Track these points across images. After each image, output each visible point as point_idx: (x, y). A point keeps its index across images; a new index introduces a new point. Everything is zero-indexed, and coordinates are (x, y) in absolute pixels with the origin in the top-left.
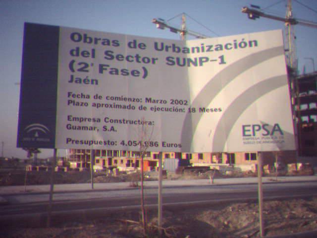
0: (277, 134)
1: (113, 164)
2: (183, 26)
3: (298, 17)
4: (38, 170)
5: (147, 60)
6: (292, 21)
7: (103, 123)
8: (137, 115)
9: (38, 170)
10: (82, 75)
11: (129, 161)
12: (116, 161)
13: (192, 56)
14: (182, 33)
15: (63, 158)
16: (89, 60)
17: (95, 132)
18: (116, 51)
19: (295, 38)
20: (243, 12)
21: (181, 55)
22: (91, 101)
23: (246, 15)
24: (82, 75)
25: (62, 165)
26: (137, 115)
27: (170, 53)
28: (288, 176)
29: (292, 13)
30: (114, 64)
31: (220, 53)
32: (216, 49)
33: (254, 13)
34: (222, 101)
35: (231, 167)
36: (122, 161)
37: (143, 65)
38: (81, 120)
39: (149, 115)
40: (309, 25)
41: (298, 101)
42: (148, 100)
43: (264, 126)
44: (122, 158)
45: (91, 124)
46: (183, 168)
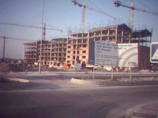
0: (135, 64)
1: (47, 64)
2: (84, 4)
3: (135, 6)
4: (18, 65)
5: (110, 48)
6: (133, 8)
7: (102, 61)
8: (108, 59)
9: (18, 65)
10: (99, 51)
11: (55, 63)
12: (48, 63)
13: (119, 47)
14: (83, 7)
15: (21, 60)
16: (100, 48)
17: (101, 62)
18: (105, 46)
19: (133, 15)
20: (113, 3)
21: (117, 47)
22: (101, 56)
23: (115, 5)
24: (99, 51)
25: (20, 63)
26: (108, 59)
27: (115, 46)
28: (116, 72)
29: (133, 5)
30: (104, 49)
31: (125, 47)
32: (124, 46)
33: (118, 4)
34: (125, 57)
35: (102, 68)
36: (51, 63)
37: (110, 49)
38: (99, 60)
39: (110, 59)
40: (139, 10)
41: (132, 42)
42: (111, 56)
43: (133, 62)
44: (52, 61)
45: (100, 61)
46: (84, 67)
